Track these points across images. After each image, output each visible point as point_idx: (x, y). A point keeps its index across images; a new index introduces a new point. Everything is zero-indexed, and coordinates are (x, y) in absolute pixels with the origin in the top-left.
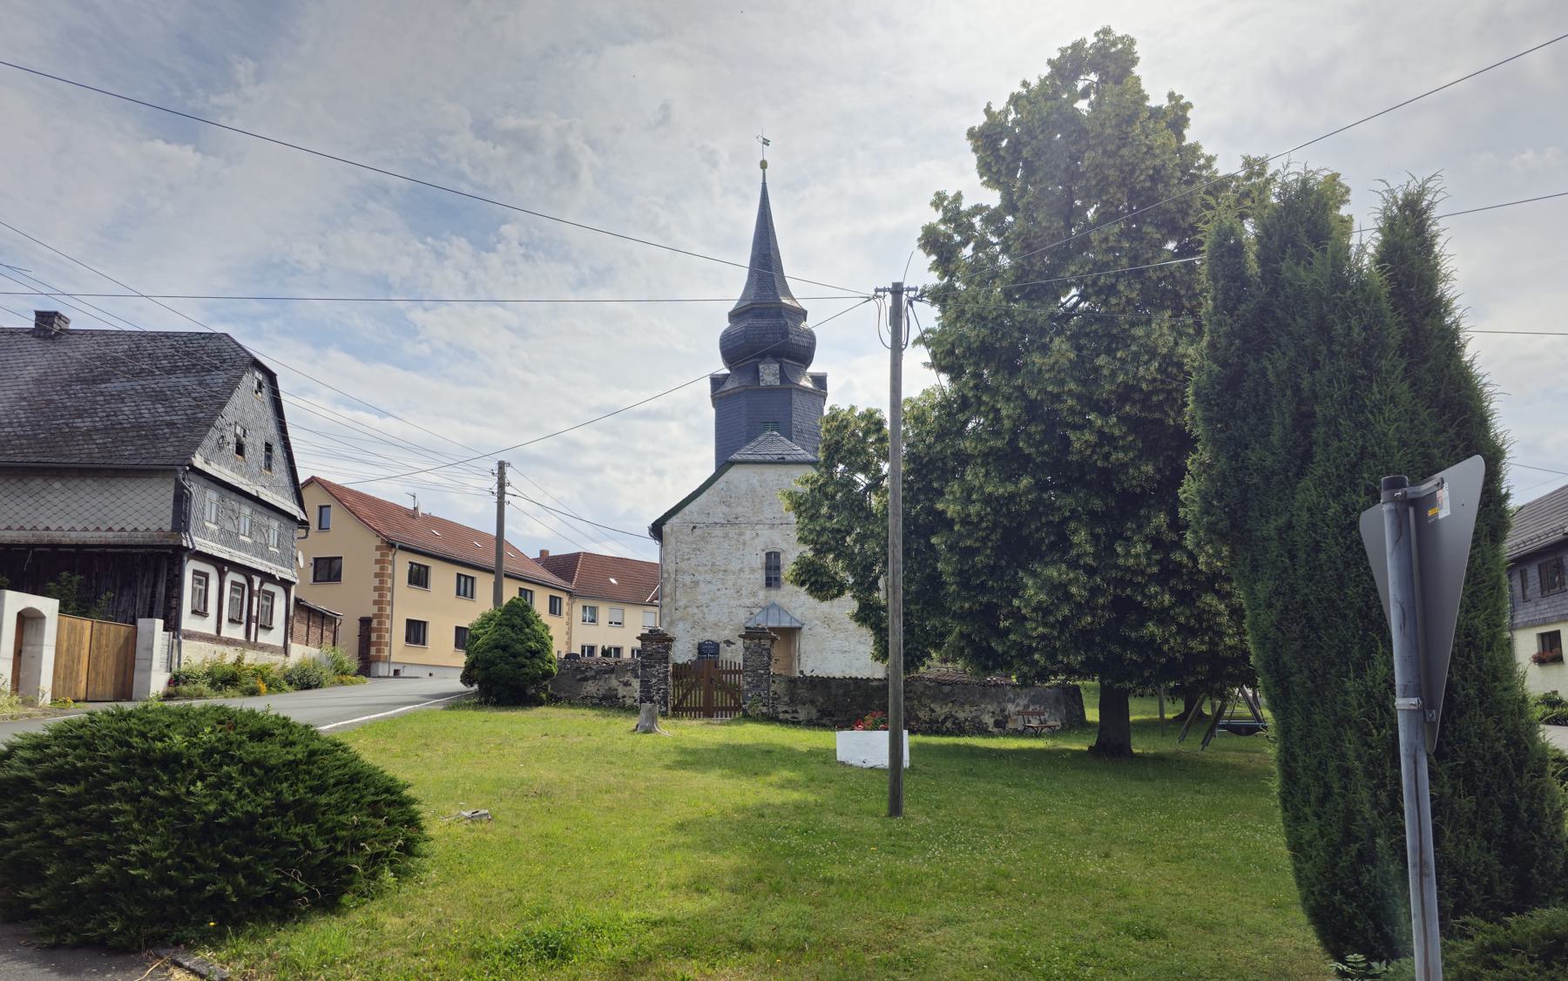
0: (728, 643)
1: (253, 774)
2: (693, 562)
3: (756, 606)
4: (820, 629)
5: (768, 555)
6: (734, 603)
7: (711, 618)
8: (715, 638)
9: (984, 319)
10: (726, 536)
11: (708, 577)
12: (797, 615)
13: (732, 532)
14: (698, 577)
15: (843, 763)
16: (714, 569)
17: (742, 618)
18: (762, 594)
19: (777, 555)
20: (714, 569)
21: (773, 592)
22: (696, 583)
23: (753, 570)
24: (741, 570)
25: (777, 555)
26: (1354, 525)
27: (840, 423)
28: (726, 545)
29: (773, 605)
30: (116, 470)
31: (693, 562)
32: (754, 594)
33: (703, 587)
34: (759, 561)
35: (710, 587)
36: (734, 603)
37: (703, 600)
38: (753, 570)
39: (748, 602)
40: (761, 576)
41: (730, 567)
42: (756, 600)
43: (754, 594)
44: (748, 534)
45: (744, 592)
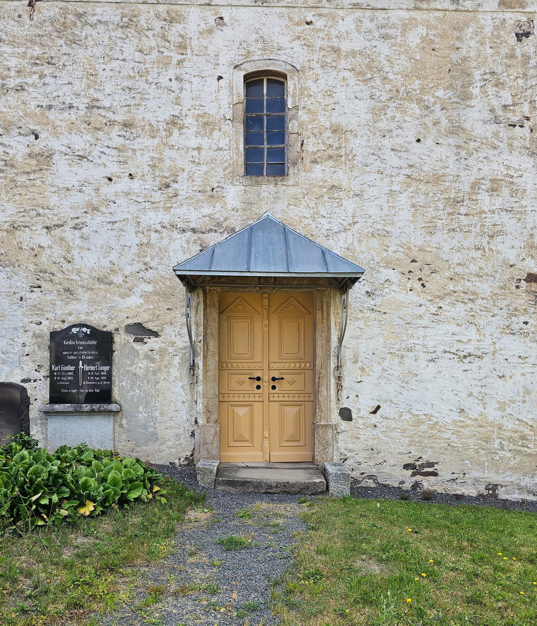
0: (140, 332)
2: (34, 97)
3: (217, 226)
4: (401, 296)
5: (252, 81)
6: (153, 218)
7: (89, 261)
8: (100, 320)
11: (79, 143)
12: (337, 246)
14: (47, 140)
15: (417, 497)
16: (93, 117)
18: (234, 193)
19: (277, 80)
20: (93, 117)
21: (267, 188)
22: (45, 158)
23: (208, 125)
24: (174, 122)
25: (277, 80)
27: (425, 493)
28: (129, 49)
29: (267, 224)
30: (58, 412)
31: (34, 97)
33: (63, 171)
34: (226, 97)
35: (84, 171)
36: (153, 218)
37: (65, 207)
38: (208, 125)
39: (195, 217)
40: (230, 141)
41: (140, 115)
42: (216, 210)
43: (213, 194)
45: (182, 186)
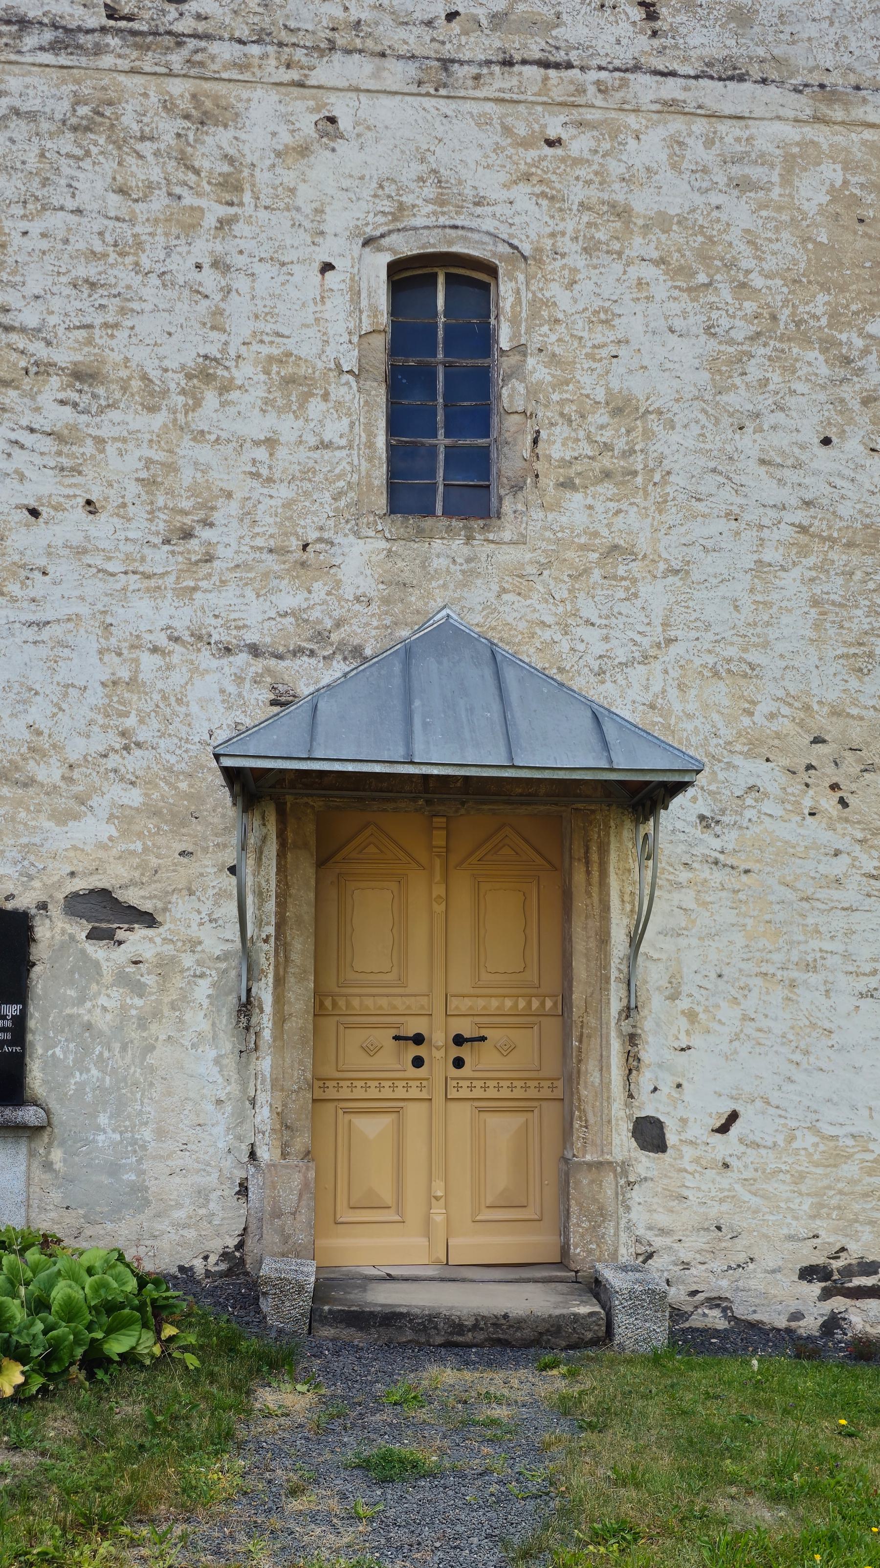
0: (106, 912)
1: (181, 1474)
3: (317, 642)
5: (409, 277)
6: (146, 615)
9: (154, 1015)
10: (93, 120)
13: (143, 95)
17: (217, 710)
18: (362, 557)
19: (473, 278)
21: (446, 548)
23: (294, 385)
24: (206, 374)
25: (473, 278)
26: (711, 1338)
28: (93, 184)
29: (447, 638)
32: (306, 559)
34: (341, 317)
36: (146, 615)
38: (294, 385)
40: (352, 428)
41: (115, 350)
42: (315, 600)
43: (306, 559)
44: (264, 119)
45: (226, 537)
